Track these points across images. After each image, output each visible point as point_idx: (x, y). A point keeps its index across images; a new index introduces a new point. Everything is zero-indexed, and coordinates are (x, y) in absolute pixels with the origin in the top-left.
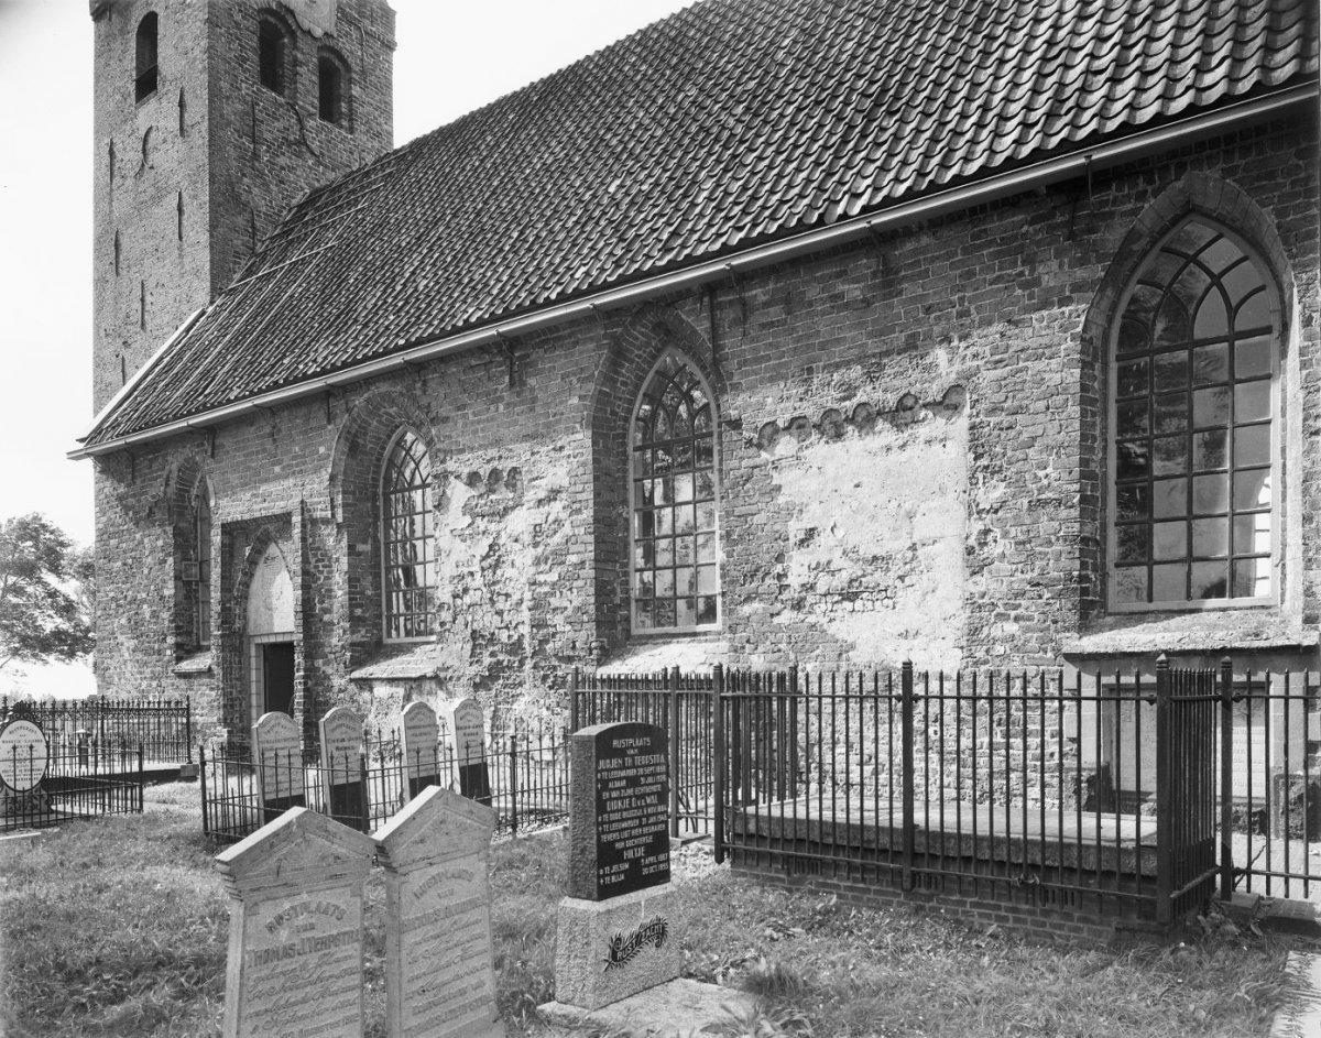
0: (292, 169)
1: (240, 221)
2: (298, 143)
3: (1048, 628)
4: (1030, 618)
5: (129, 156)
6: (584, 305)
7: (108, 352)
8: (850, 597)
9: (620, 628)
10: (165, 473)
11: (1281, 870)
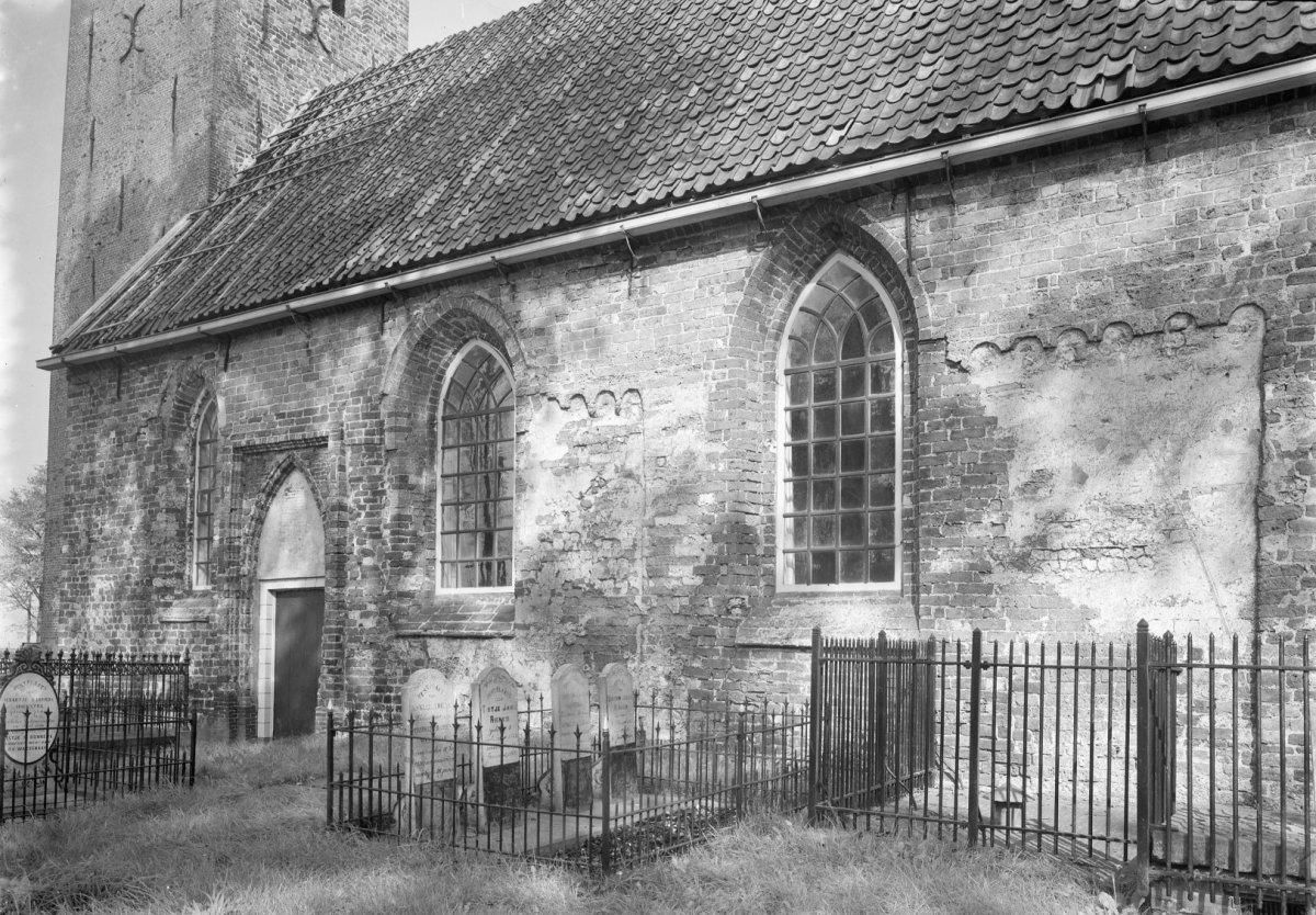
0: (300, 63)
1: (244, 114)
2: (310, 36)
6: (743, 198)
9: (762, 584)
10: (163, 387)
11: (1103, 833)
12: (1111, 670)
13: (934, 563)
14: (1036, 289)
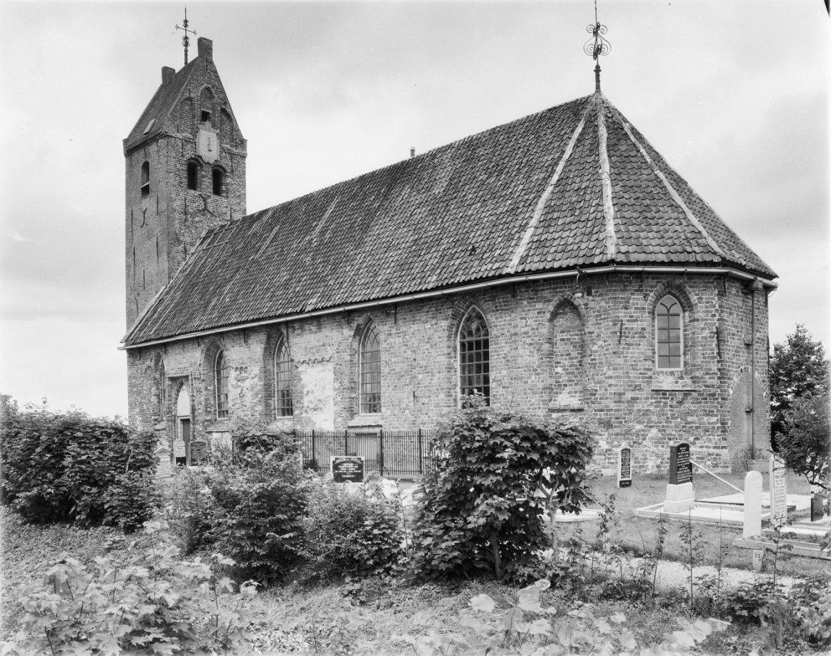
2: (204, 210)
5: (138, 216)
7: (132, 297)
8: (315, 410)
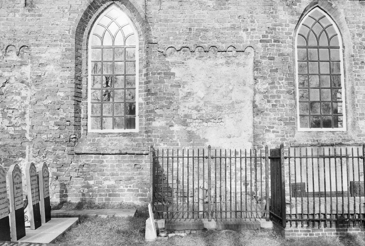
3: (284, 136)
4: (278, 132)
11: (354, 159)
12: (236, 158)
13: (153, 122)
14: (188, 31)
